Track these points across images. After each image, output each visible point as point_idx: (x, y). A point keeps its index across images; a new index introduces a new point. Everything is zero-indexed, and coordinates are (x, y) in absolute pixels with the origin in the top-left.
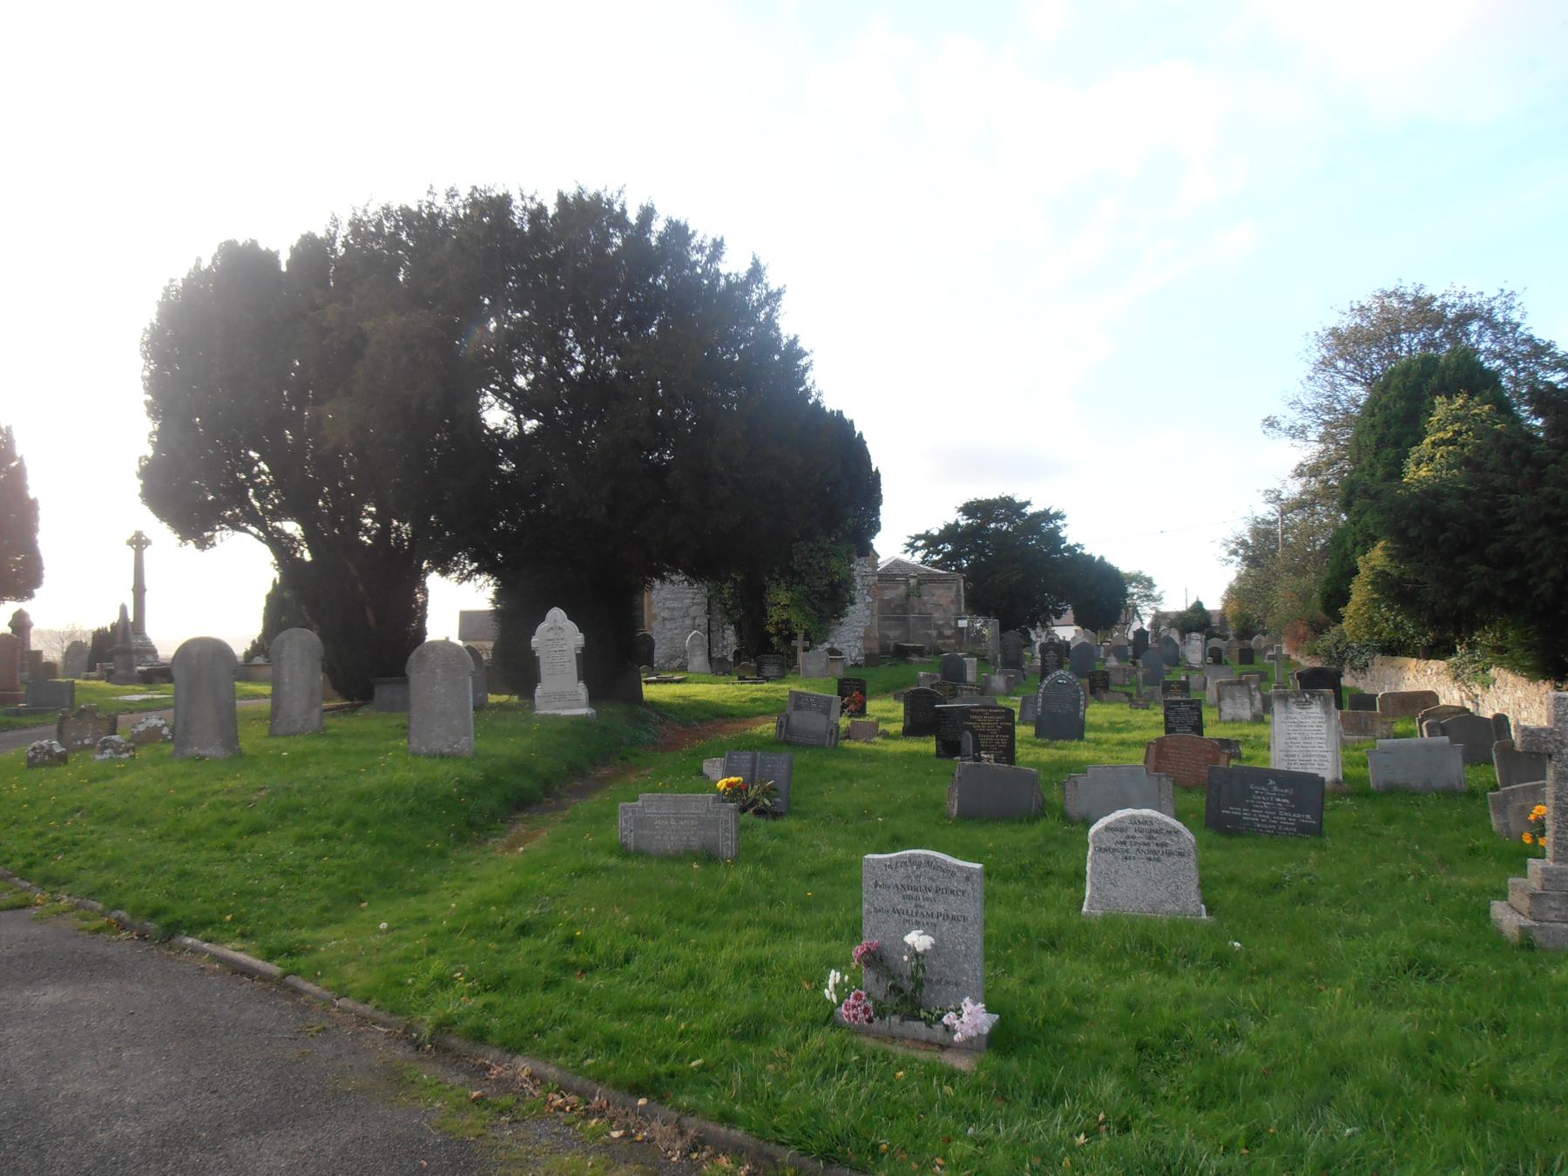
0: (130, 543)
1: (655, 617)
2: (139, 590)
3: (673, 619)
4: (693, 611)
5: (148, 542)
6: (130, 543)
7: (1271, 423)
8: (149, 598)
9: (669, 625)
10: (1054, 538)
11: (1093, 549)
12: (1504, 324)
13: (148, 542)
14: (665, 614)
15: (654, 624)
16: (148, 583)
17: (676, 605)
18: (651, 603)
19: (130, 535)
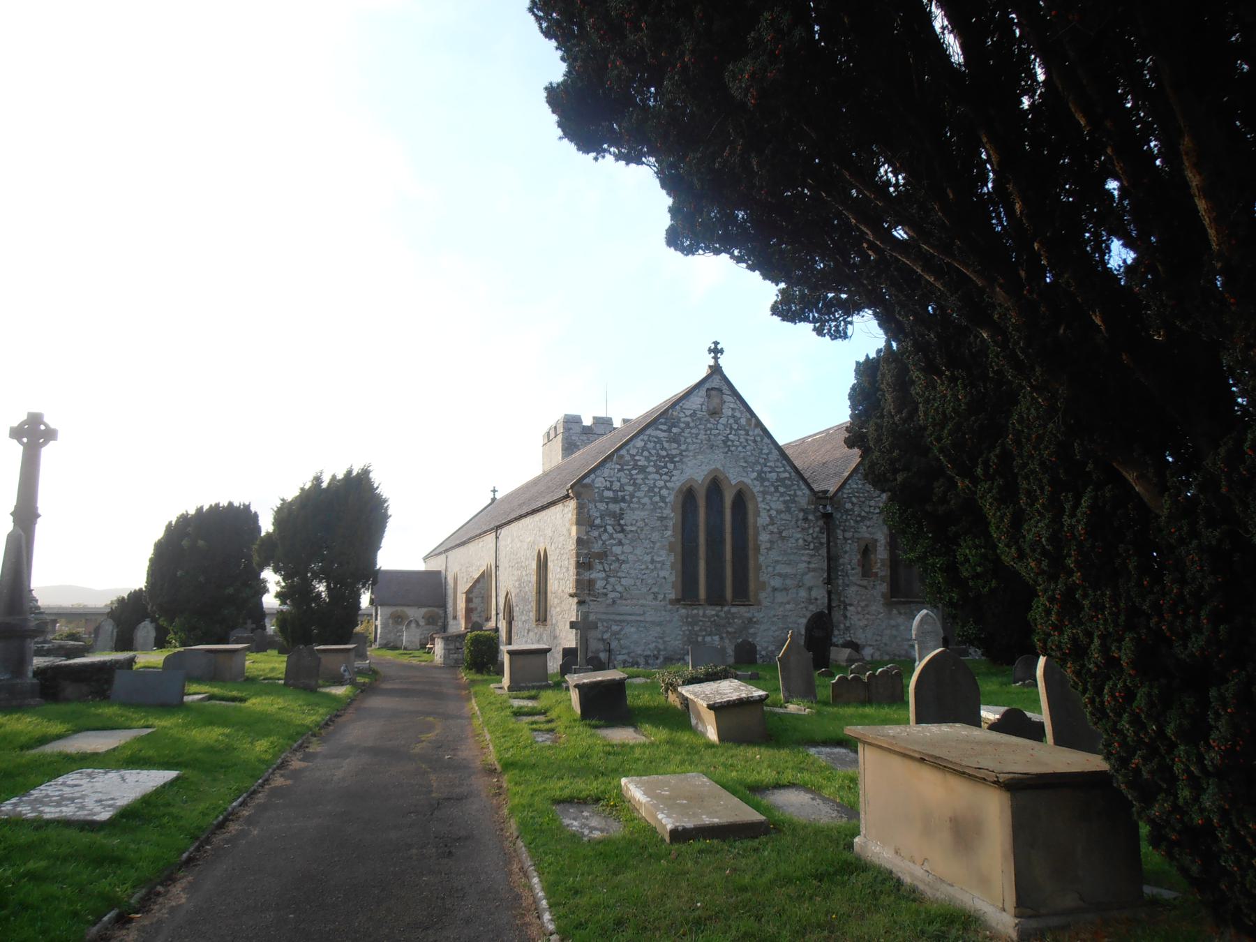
0: (16, 433)
1: (762, 586)
2: (26, 515)
3: (786, 589)
4: (809, 580)
5: (50, 435)
6: (16, 433)
7: (716, 351)
8: (42, 530)
9: (780, 597)
10: (291, 503)
11: (145, 579)
12: (802, 310)
13: (50, 435)
14: (776, 582)
15: (763, 595)
16: (43, 504)
17: (788, 570)
18: (758, 568)
19: (51, 420)
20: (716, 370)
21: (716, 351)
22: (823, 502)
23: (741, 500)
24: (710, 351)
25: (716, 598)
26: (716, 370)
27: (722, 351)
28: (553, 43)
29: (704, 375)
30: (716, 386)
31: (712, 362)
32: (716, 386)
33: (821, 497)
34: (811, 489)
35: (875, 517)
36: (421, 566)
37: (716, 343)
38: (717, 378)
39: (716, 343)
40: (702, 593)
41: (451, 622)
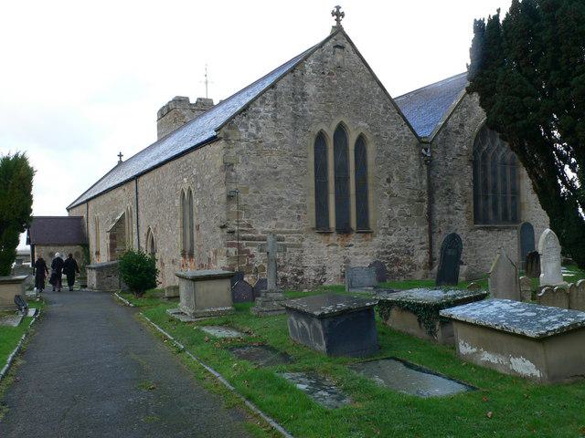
7: (338, 14)
20: (338, 31)
21: (338, 14)
22: (425, 146)
23: (361, 141)
24: (333, 14)
25: (344, 230)
26: (338, 31)
27: (343, 15)
28: (31, 165)
29: (328, 34)
30: (339, 39)
31: (335, 24)
32: (339, 39)
33: (421, 142)
34: (416, 135)
35: (461, 213)
36: (65, 214)
37: (338, 8)
38: (339, 35)
39: (338, 8)
40: (332, 224)
41: (93, 255)
